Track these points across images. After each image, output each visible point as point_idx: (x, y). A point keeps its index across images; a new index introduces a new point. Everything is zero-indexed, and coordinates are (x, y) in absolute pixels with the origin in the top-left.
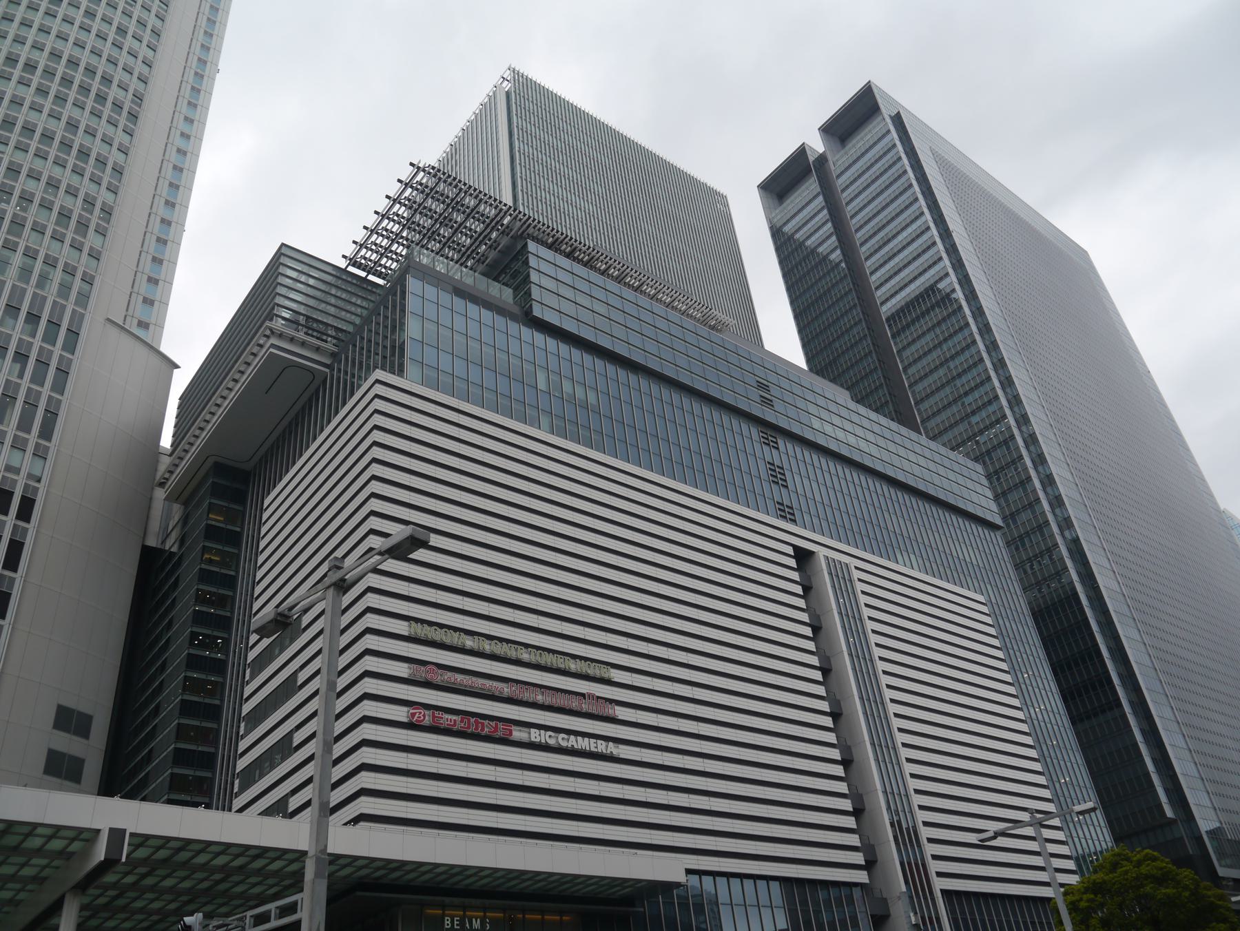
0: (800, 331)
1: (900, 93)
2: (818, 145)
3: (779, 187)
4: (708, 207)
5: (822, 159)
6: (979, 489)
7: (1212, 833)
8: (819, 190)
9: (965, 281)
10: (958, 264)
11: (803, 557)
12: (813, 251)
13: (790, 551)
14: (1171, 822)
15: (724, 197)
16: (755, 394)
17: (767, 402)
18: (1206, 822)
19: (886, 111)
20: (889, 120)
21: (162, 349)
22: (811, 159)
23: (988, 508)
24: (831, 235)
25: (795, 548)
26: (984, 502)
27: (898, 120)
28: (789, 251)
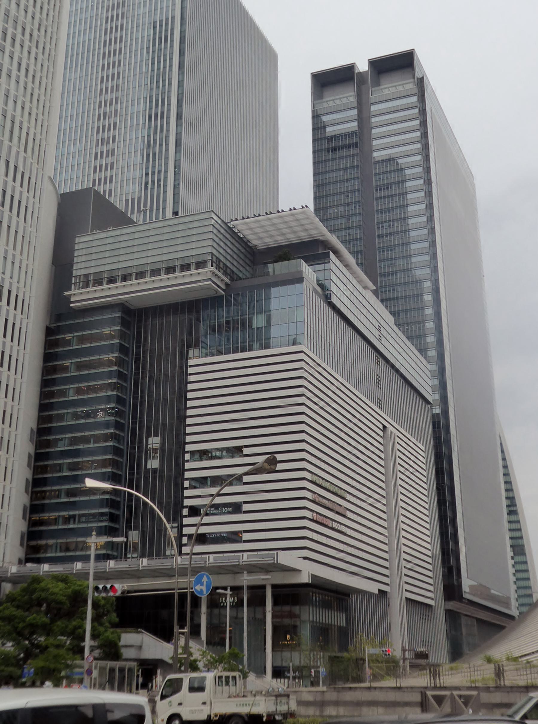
1: (427, 64)
2: (363, 67)
3: (326, 81)
4: (263, 58)
17: (380, 340)
22: (356, 71)
24: (352, 108)
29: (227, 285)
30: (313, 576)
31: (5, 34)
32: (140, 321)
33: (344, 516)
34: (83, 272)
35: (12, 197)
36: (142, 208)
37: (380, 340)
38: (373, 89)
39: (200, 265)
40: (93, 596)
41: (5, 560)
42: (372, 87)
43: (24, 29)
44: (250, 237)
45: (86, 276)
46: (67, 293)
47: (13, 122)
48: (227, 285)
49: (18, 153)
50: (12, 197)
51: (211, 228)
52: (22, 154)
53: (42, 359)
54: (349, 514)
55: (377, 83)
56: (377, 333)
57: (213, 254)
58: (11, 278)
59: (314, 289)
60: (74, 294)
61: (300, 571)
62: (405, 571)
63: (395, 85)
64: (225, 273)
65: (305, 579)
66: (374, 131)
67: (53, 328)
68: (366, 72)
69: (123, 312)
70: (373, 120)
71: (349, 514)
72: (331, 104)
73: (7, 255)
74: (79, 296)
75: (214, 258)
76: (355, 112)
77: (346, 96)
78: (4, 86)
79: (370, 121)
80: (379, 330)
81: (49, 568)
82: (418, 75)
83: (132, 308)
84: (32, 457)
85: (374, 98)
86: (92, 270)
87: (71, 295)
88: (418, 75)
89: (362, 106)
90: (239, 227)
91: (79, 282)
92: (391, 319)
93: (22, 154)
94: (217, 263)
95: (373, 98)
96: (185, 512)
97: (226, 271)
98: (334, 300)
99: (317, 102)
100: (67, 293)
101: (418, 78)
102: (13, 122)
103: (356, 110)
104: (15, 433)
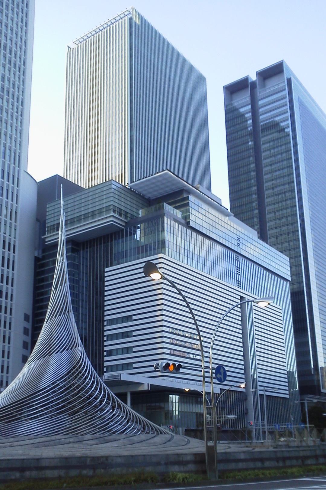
0: (228, 142)
1: (296, 68)
2: (253, 77)
3: (233, 90)
4: (198, 82)
6: (284, 261)
7: (322, 368)
8: (250, 102)
9: (294, 130)
10: (293, 123)
11: (242, 298)
12: (237, 110)
13: (239, 297)
14: (313, 375)
16: (236, 242)
17: (239, 245)
18: (321, 364)
19: (286, 75)
20: (286, 81)
21: (28, 172)
22: (249, 81)
23: (287, 274)
24: (248, 105)
26: (285, 271)
27: (289, 81)
28: (232, 118)
31: (3, 88)
34: (52, 223)
35: (13, 176)
43: (18, 99)
44: (144, 193)
47: (15, 153)
49: (14, 168)
50: (13, 176)
51: (112, 194)
52: (12, 165)
55: (264, 86)
58: (15, 238)
62: (258, 362)
63: (273, 84)
66: (261, 117)
68: (256, 81)
69: (72, 244)
70: (260, 110)
77: (244, 98)
78: (3, 141)
93: (12, 165)
96: (105, 354)
102: (15, 153)
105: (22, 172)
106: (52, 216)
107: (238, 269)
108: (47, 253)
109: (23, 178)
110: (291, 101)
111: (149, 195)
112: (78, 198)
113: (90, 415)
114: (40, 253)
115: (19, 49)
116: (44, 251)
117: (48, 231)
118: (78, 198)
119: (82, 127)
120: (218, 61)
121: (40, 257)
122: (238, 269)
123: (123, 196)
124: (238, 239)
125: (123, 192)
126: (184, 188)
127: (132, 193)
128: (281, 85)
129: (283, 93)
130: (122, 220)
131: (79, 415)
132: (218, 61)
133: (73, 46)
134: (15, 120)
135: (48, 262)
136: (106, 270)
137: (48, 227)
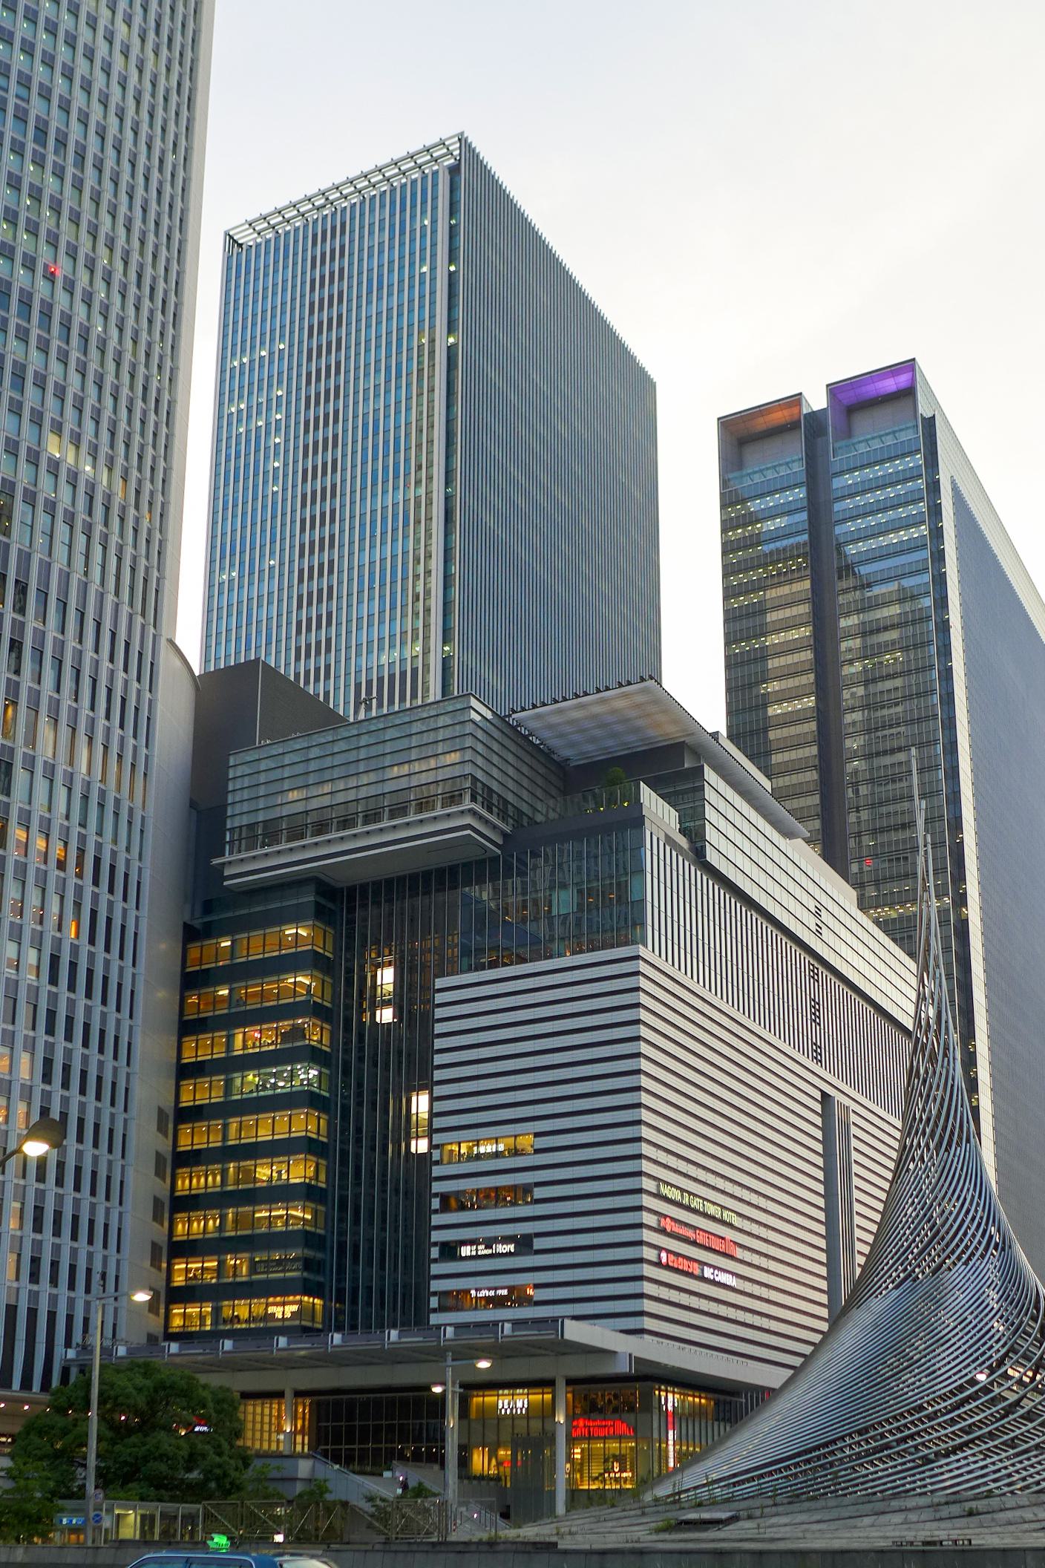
1: (950, 393)
2: (817, 401)
3: (743, 436)
5: (814, 417)
13: (818, 1095)
15: (653, 385)
17: (818, 933)
25: (824, 1094)
27: (930, 423)
29: (505, 835)
30: (639, 1361)
32: (351, 910)
33: (731, 1257)
34: (245, 820)
36: (363, 696)
37: (818, 933)
38: (837, 445)
39: (453, 798)
40: (554, 1394)
41: (118, 1337)
42: (835, 440)
44: (554, 743)
45: (251, 826)
46: (216, 861)
48: (505, 835)
53: (178, 983)
54: (740, 1253)
55: (847, 432)
56: (811, 921)
57: (475, 779)
59: (669, 840)
60: (230, 863)
61: (615, 1352)
63: (873, 432)
64: (503, 815)
65: (623, 1367)
67: (198, 926)
69: (318, 893)
70: (838, 507)
71: (740, 1253)
72: (758, 478)
73: (88, 791)
74: (244, 865)
75: (479, 785)
76: (800, 493)
79: (831, 510)
80: (817, 914)
81: (180, 1349)
82: (924, 410)
83: (339, 885)
84: (165, 1160)
85: (842, 463)
86: (261, 817)
87: (224, 864)
88: (924, 410)
89: (815, 478)
90: (534, 725)
91: (240, 840)
92: (848, 896)
94: (485, 796)
95: (836, 461)
97: (504, 810)
98: (712, 857)
99: (731, 476)
100: (216, 861)
101: (923, 419)
103: (804, 489)
104: (124, 1115)
105: (163, 642)
106: (246, 794)
107: (815, 1004)
108: (216, 918)
109: (166, 661)
110: (934, 487)
111: (567, 753)
112: (342, 746)
113: (902, 1464)
114: (197, 914)
115: (141, 180)
116: (208, 907)
117: (231, 842)
118: (342, 746)
119: (283, 514)
120: (711, 331)
121: (197, 923)
122: (815, 1004)
123: (495, 747)
124: (817, 914)
125: (496, 734)
126: (687, 740)
127: (520, 740)
128: (903, 437)
129: (910, 462)
130: (495, 827)
131: (941, 1466)
132: (711, 331)
133: (247, 238)
134: (121, 448)
135: (483, 936)
136: (440, 983)
137: (232, 829)
